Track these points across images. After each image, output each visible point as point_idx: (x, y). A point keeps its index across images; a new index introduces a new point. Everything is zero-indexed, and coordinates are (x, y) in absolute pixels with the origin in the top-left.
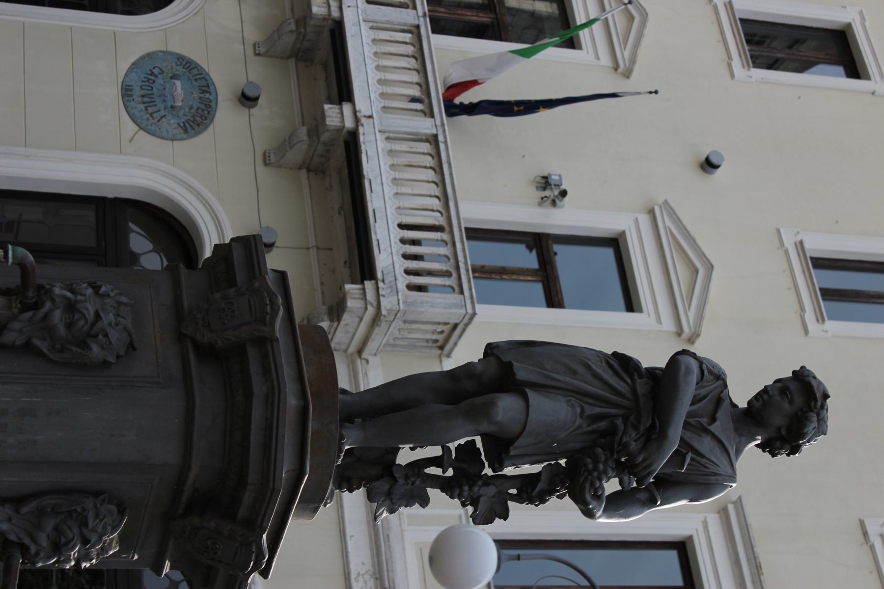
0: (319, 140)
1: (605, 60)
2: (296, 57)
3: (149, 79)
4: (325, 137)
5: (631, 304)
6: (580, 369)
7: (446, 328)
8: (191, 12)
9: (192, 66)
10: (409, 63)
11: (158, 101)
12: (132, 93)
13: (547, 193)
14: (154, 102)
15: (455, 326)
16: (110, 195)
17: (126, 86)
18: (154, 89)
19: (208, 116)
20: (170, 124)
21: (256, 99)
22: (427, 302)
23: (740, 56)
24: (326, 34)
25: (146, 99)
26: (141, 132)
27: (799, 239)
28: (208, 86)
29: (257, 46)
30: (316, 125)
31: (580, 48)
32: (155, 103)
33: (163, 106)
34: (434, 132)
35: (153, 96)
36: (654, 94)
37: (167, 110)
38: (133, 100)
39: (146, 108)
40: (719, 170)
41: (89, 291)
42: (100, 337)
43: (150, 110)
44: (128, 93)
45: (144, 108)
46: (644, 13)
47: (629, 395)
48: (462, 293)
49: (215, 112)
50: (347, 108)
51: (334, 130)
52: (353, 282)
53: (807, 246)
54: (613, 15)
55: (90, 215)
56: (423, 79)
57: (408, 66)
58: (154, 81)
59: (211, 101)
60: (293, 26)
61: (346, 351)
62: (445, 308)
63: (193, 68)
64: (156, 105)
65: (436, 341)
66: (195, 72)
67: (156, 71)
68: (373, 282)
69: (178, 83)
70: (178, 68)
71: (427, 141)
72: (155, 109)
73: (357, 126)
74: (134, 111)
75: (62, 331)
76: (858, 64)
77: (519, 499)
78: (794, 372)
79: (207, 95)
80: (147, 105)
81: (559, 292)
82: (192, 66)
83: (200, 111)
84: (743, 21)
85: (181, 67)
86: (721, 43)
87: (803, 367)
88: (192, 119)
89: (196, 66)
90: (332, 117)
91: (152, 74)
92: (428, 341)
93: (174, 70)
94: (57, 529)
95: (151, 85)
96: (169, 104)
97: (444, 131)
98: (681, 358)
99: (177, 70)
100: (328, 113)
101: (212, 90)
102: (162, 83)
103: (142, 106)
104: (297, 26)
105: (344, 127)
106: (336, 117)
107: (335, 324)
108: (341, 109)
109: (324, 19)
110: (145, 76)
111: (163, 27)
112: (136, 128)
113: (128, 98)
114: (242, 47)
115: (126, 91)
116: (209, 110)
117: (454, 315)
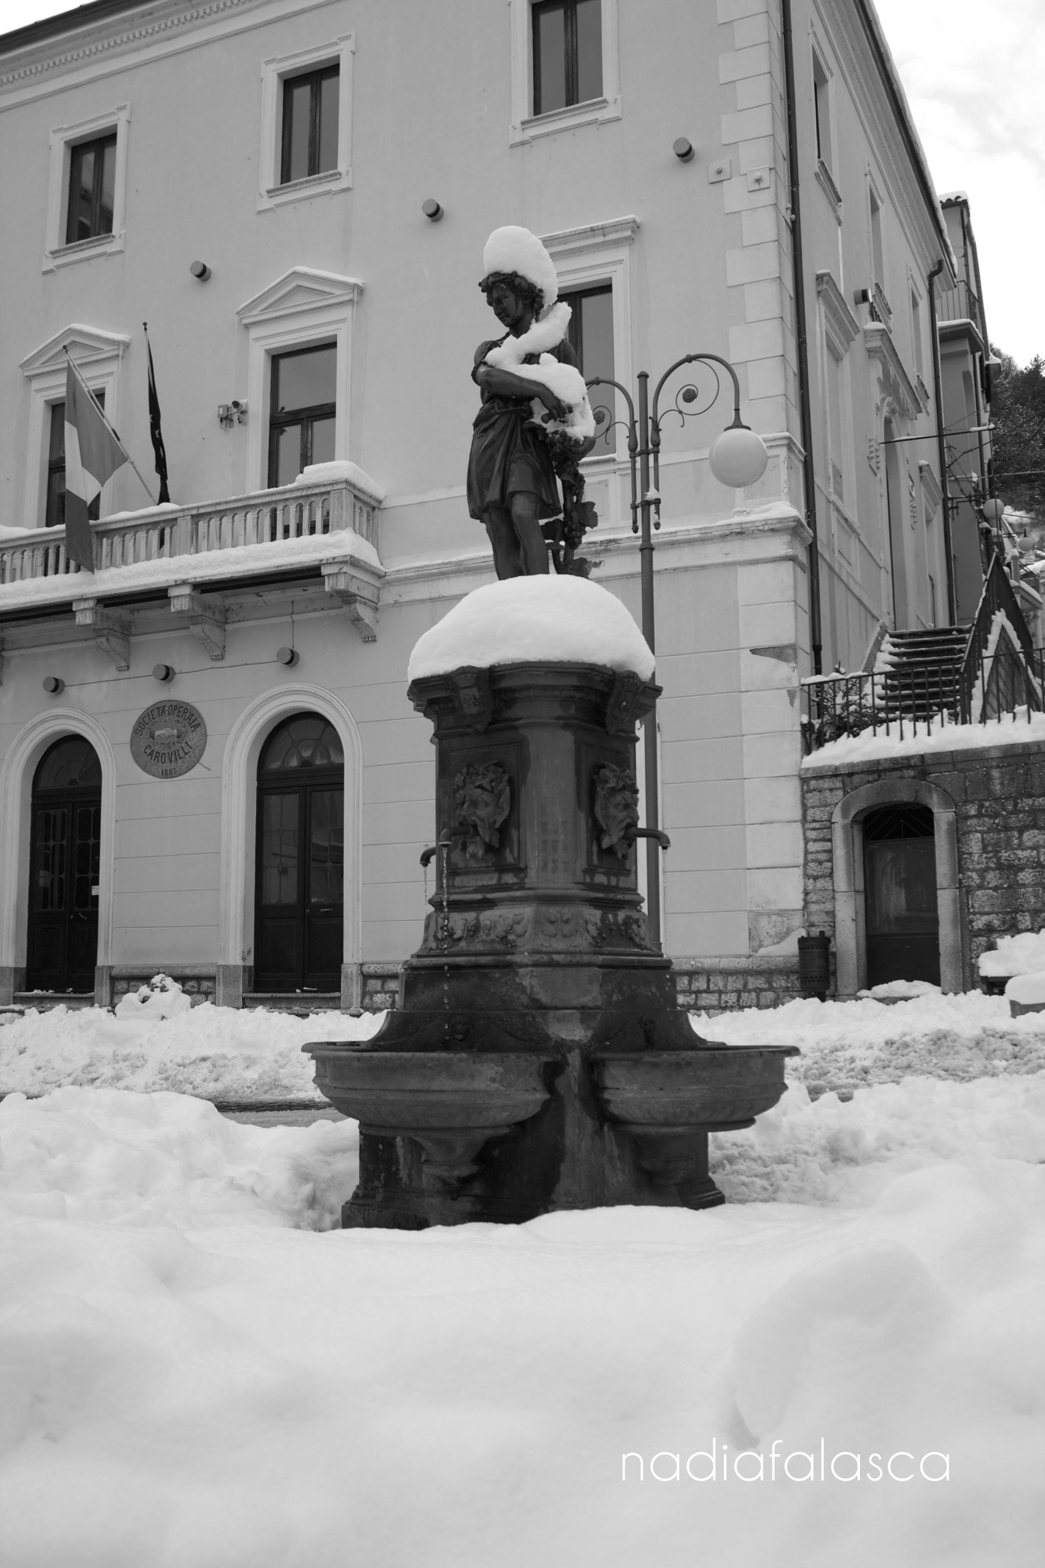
4: (199, 611)
5: (330, 345)
6: (489, 452)
7: (358, 505)
10: (130, 540)
11: (174, 748)
13: (235, 418)
15: (355, 496)
16: (255, 784)
20: (192, 738)
22: (338, 522)
23: (102, 244)
25: (173, 759)
26: (201, 761)
27: (264, 194)
28: (158, 708)
30: (188, 619)
33: (178, 745)
40: (208, 266)
41: (461, 792)
42: (493, 784)
43: (182, 755)
47: (508, 416)
48: (328, 493)
50: (172, 593)
52: (324, 584)
53: (271, 187)
54: (75, 359)
55: (274, 800)
56: (143, 527)
60: (103, 639)
61: (379, 589)
62: (342, 507)
65: (368, 515)
66: (147, 720)
68: (322, 568)
69: (157, 733)
71: (197, 524)
72: (181, 751)
73: (188, 583)
74: (184, 768)
75: (490, 808)
76: (102, 135)
77: (580, 495)
78: (483, 291)
79: (166, 708)
81: (321, 407)
83: (180, 714)
84: (69, 240)
86: (91, 262)
87: (480, 285)
92: (368, 520)
94: (616, 807)
96: (176, 739)
97: (188, 509)
98: (479, 381)
101: (162, 705)
103: (180, 761)
104: (102, 636)
107: (358, 598)
108: (175, 597)
109: (96, 613)
112: (198, 764)
115: (167, 774)
117: (347, 498)
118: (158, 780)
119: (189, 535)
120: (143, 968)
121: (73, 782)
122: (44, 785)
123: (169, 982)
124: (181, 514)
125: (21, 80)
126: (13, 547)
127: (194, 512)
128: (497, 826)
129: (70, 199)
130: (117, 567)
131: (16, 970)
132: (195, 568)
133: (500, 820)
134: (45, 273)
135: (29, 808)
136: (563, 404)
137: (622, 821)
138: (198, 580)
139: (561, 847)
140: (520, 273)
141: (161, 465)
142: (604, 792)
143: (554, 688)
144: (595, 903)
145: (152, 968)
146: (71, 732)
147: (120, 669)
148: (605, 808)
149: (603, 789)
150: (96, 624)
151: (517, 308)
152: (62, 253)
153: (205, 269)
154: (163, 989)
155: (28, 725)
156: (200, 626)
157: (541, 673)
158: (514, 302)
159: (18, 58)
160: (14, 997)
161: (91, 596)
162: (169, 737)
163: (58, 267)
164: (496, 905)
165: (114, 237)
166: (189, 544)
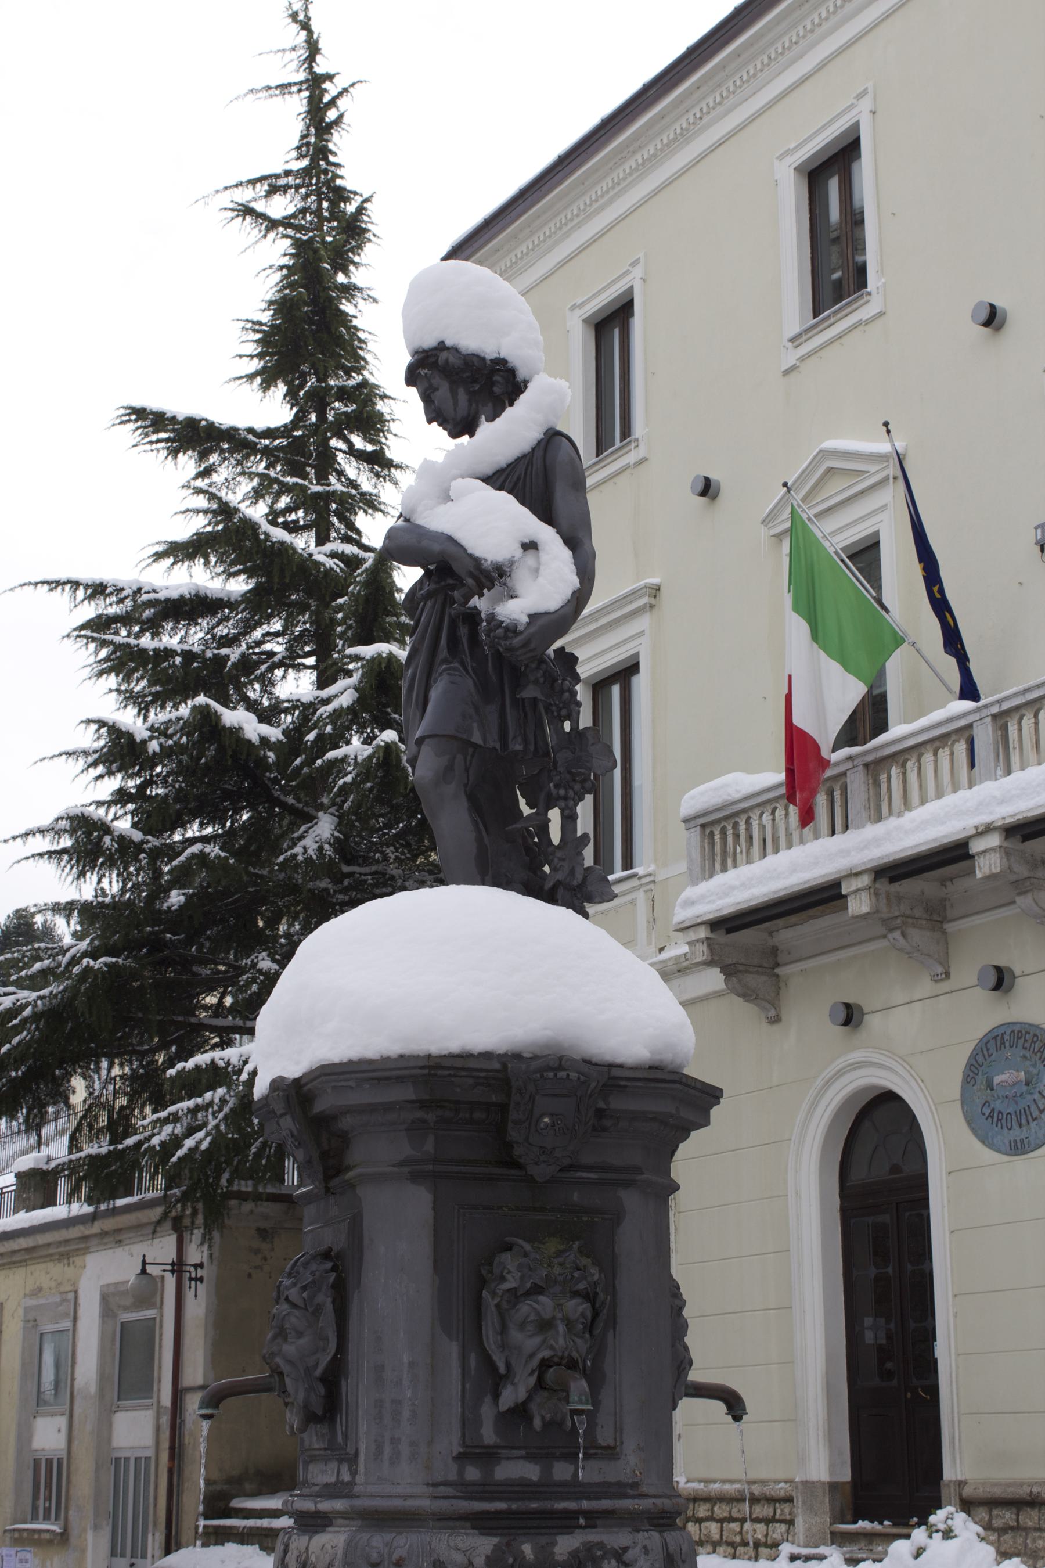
0: (1029, 878)
1: (643, 623)
2: (942, 922)
3: (998, 1120)
4: (1022, 871)
8: (908, 1071)
9: (974, 1063)
11: (1023, 1104)
12: (1018, 1141)
14: (1024, 1109)
17: (1011, 1149)
18: (1008, 1111)
19: (1032, 1034)
21: (999, 970)
24: (897, 887)
25: (1024, 1122)
28: (995, 1038)
29: (936, 978)
31: (877, 533)
32: (1027, 1108)
33: (1029, 1097)
34: (989, 719)
35: (1018, 1112)
36: (889, 427)
37: (1032, 1091)
38: (1027, 1138)
39: (1034, 1119)
43: (1036, 1113)
44: (1019, 1146)
45: (1035, 1122)
46: (821, 455)
49: (1025, 1024)
50: (976, 847)
51: (1008, 860)
56: (928, 746)
57: (916, 769)
58: (1000, 1112)
59: (1013, 1031)
60: (897, 934)
63: (977, 1061)
64: (1028, 1106)
66: (980, 1059)
67: (987, 1111)
69: (997, 1079)
70: (978, 1082)
71: (1004, 729)
72: (1033, 1107)
73: (995, 829)
79: (1006, 1037)
80: (1030, 1117)
82: (974, 1063)
85: (977, 1077)
88: (1039, 1054)
89: (973, 1056)
90: (990, 865)
91: (991, 1116)
93: (982, 1087)
94: (522, 1326)
95: (1005, 1116)
96: (1025, 1088)
99: (982, 1083)
100: (986, 871)
101: (1000, 1032)
102: (999, 1101)
103: (1033, 1124)
104: (896, 928)
105: (1000, 847)
106: (990, 859)
109: (876, 894)
110: (994, 1125)
111: (933, 1107)
113: (1027, 1146)
114: (941, 997)
115: (1018, 1148)
116: (1024, 1032)
118: (1006, 1158)
119: (992, 747)
120: (1009, 1485)
121: (895, 1169)
122: (859, 1174)
123: (961, 1521)
124: (977, 716)
125: (732, 96)
126: (759, 805)
127: (995, 710)
128: (318, 1372)
129: (812, 253)
130: (900, 815)
131: (833, 1487)
132: (1002, 802)
133: (325, 1359)
134: (786, 372)
135: (837, 1216)
136: (486, 565)
137: (532, 1355)
138: (1008, 821)
139: (406, 1413)
140: (449, 343)
141: (953, 641)
142: (497, 1300)
143: (388, 1107)
144: (482, 1523)
145: (1021, 1485)
146: (882, 1088)
147: (936, 979)
148: (503, 1329)
149: (494, 1294)
150: (877, 911)
151: (456, 403)
152: (804, 338)
153: (993, 310)
154: (948, 1534)
155: (819, 1082)
156: (1029, 895)
157: (352, 1083)
158: (448, 395)
159: (722, 66)
160: (832, 1533)
161: (863, 868)
162: (1014, 1085)
163: (802, 359)
164: (331, 1525)
165: (869, 294)
166: (992, 764)
